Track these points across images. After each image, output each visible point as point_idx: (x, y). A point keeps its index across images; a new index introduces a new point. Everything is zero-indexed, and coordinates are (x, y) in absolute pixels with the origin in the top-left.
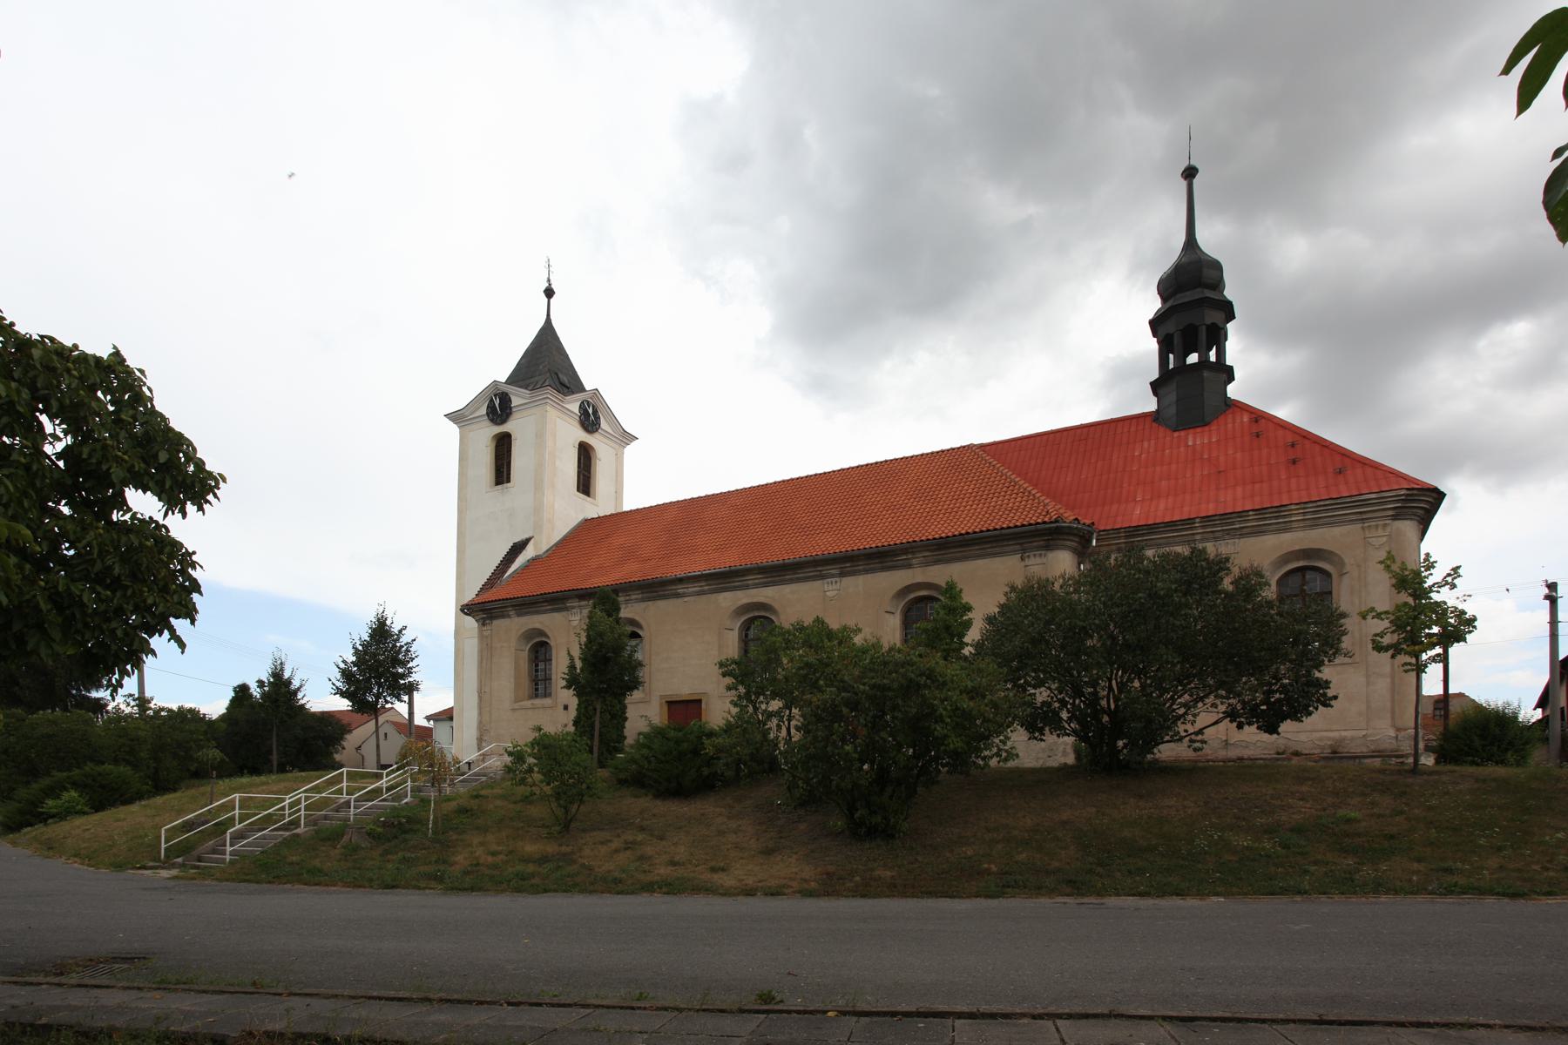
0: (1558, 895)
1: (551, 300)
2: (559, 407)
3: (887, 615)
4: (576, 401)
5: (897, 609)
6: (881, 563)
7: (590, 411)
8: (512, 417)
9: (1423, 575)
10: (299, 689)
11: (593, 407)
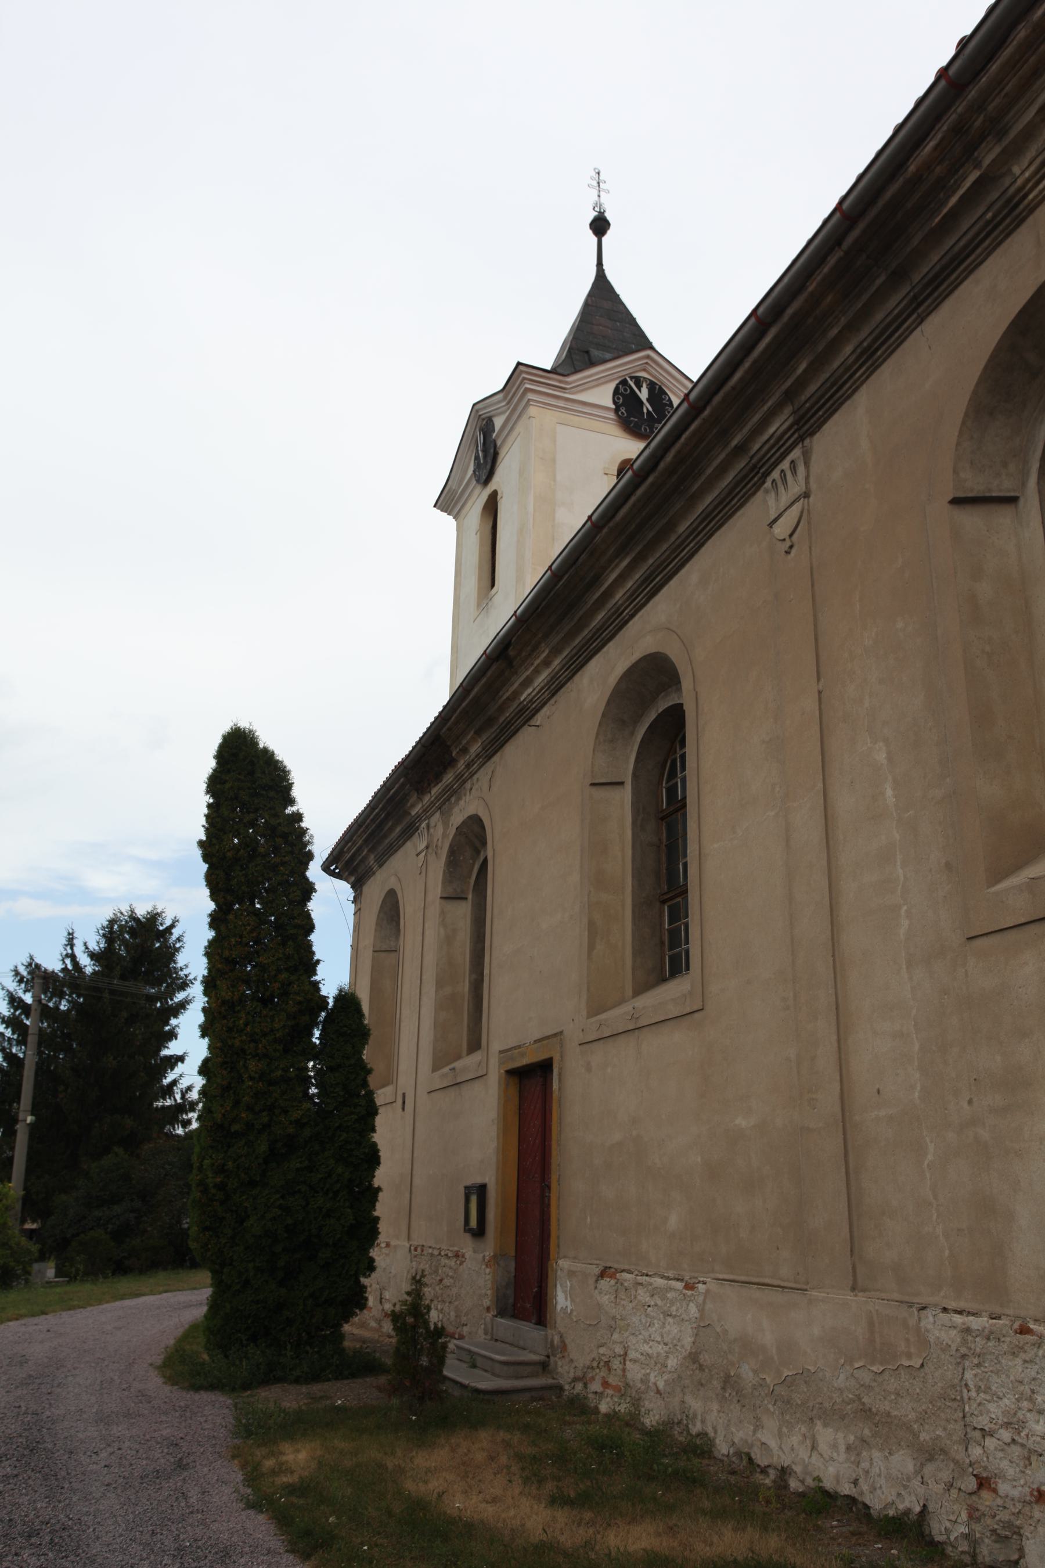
0: (596, 581)
1: (605, 239)
2: (561, 403)
3: (971, 519)
4: (599, 383)
5: (1025, 475)
6: (899, 276)
7: (644, 394)
8: (502, 453)
9: (179, 1101)
10: (172, 926)
11: (652, 386)
